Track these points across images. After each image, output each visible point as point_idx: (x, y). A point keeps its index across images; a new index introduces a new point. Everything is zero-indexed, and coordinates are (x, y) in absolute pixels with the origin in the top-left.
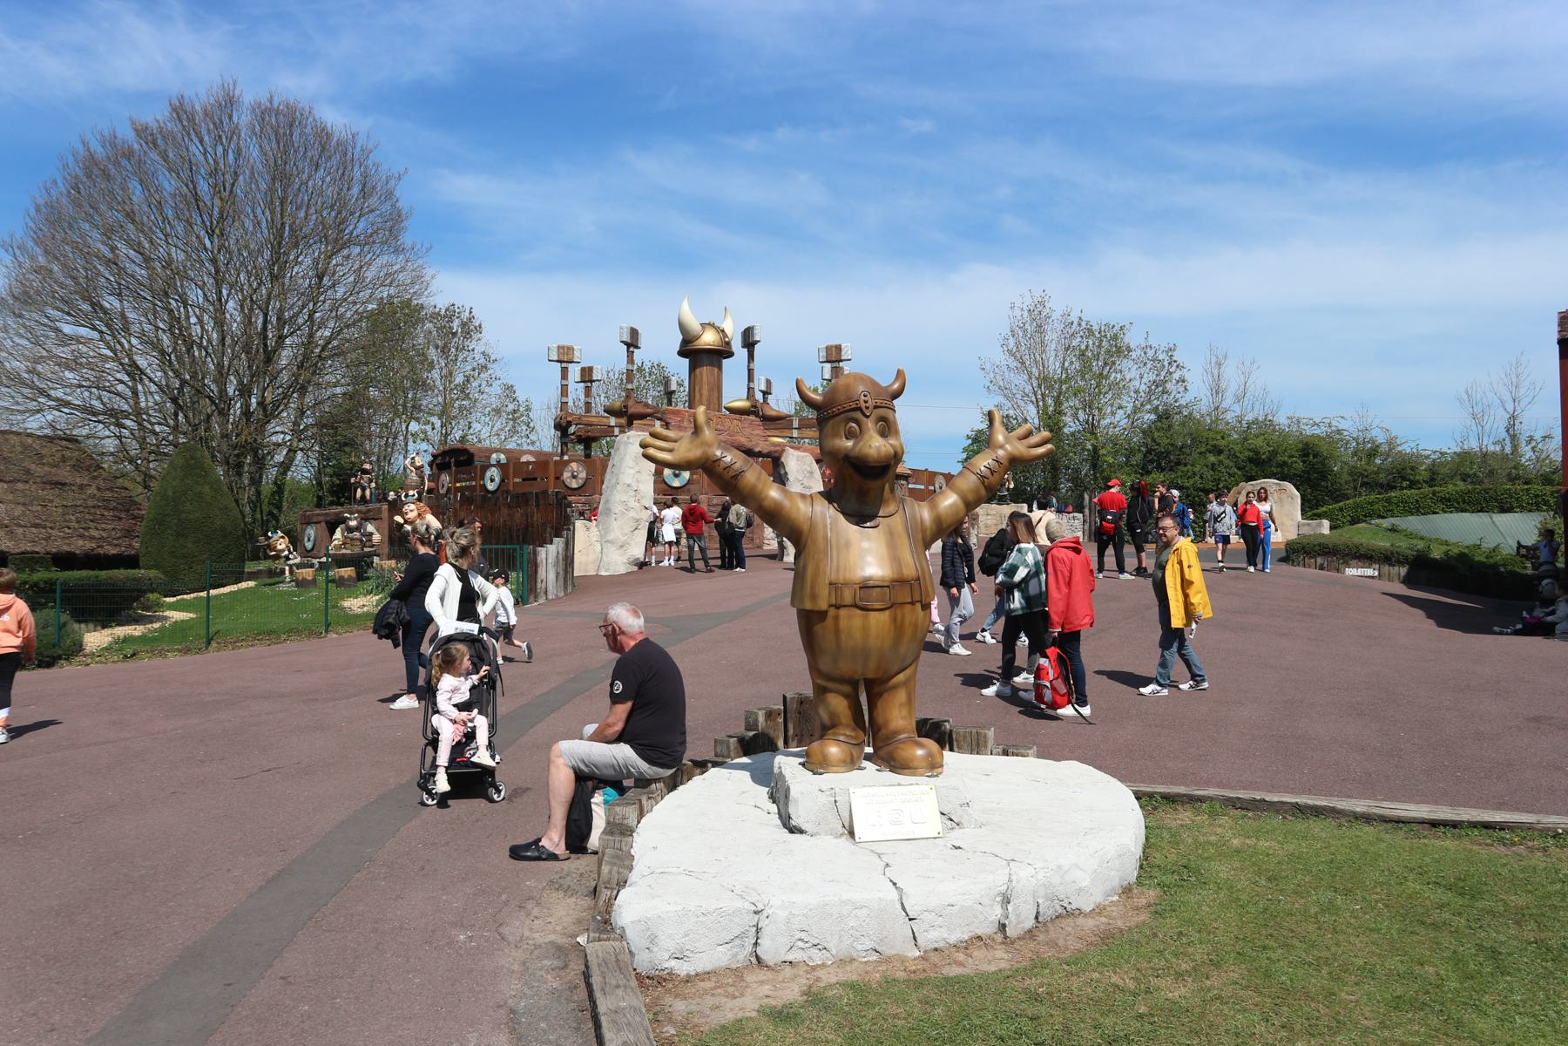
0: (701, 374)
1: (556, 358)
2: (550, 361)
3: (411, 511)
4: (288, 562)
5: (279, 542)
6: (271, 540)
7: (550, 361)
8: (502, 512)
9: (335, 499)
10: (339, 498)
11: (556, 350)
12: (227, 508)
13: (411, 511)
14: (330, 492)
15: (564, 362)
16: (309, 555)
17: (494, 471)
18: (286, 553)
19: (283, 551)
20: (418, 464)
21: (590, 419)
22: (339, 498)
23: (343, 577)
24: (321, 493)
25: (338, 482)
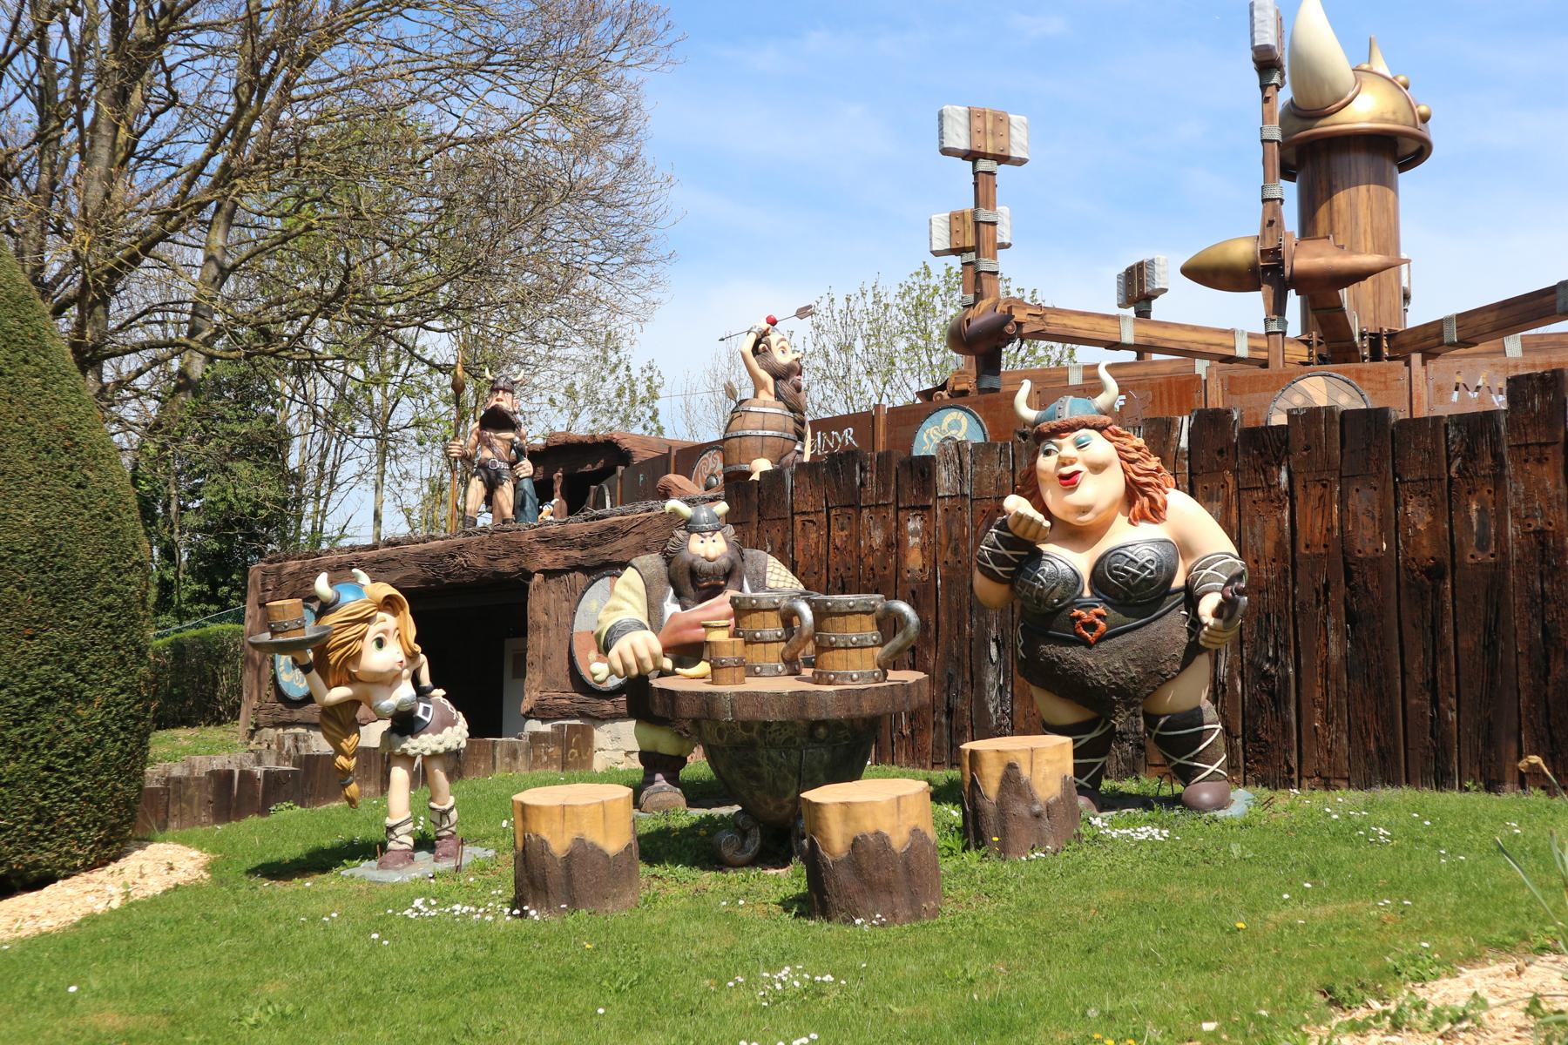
0: (1352, 205)
1: (963, 144)
2: (946, 152)
3: (1097, 468)
4: (413, 745)
5: (373, 631)
6: (330, 620)
7: (946, 152)
8: (1515, 488)
9: (206, 588)
10: (214, 586)
11: (964, 120)
12: (72, 446)
13: (1097, 468)
14: (193, 573)
15: (985, 156)
16: (298, 714)
17: (956, 425)
18: (405, 691)
19: (388, 680)
20: (783, 359)
21: (1066, 321)
22: (214, 586)
23: (882, 839)
24: (169, 575)
25: (216, 546)
